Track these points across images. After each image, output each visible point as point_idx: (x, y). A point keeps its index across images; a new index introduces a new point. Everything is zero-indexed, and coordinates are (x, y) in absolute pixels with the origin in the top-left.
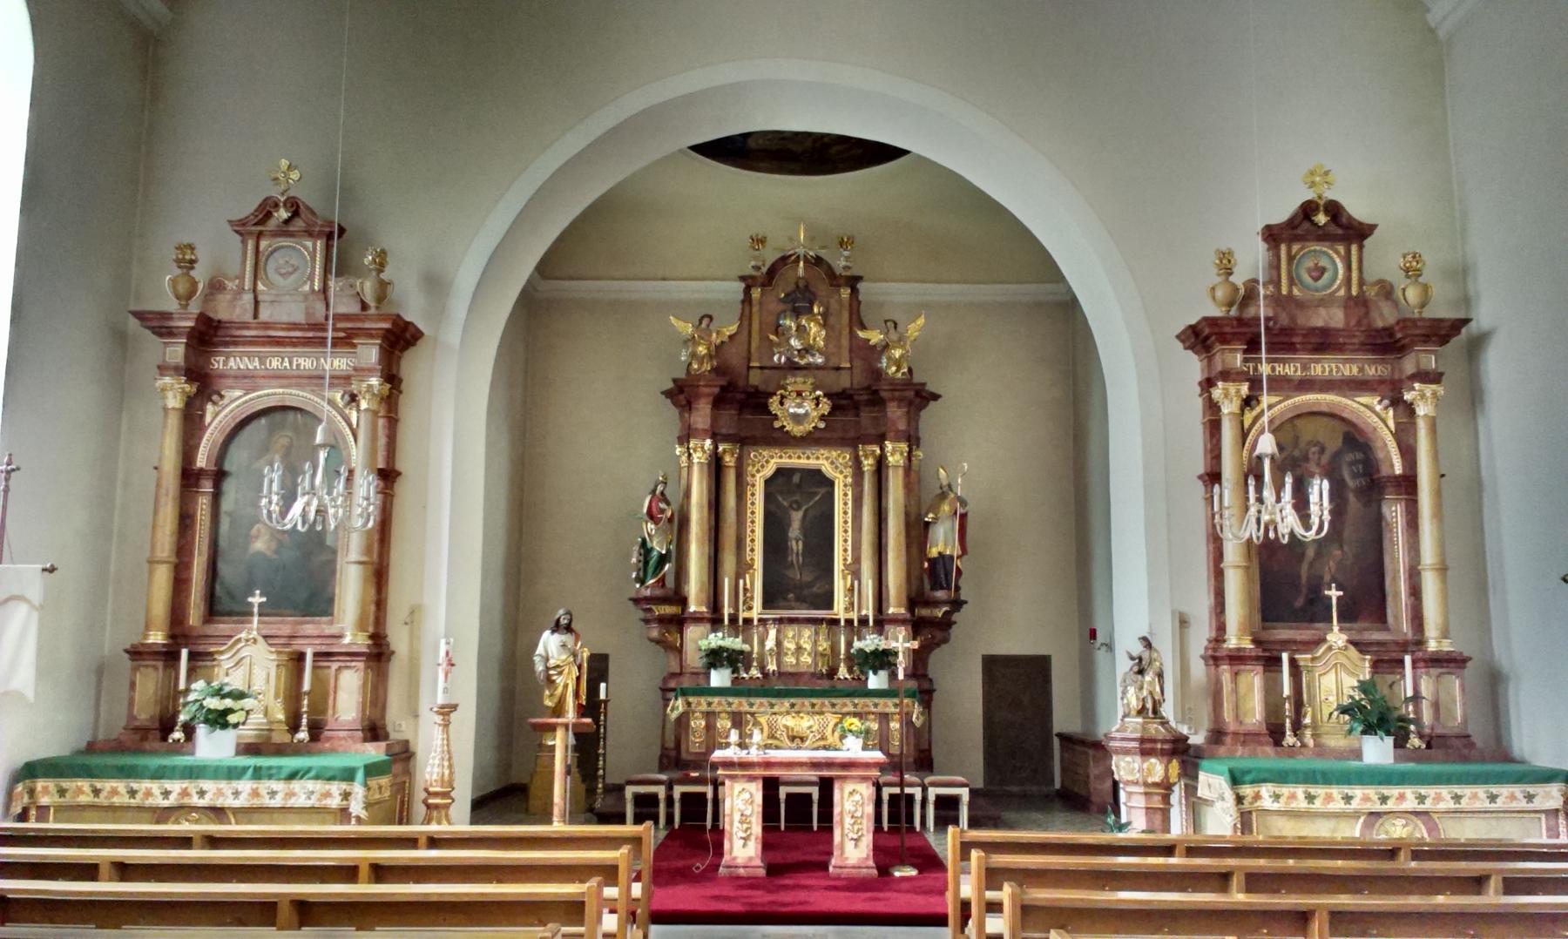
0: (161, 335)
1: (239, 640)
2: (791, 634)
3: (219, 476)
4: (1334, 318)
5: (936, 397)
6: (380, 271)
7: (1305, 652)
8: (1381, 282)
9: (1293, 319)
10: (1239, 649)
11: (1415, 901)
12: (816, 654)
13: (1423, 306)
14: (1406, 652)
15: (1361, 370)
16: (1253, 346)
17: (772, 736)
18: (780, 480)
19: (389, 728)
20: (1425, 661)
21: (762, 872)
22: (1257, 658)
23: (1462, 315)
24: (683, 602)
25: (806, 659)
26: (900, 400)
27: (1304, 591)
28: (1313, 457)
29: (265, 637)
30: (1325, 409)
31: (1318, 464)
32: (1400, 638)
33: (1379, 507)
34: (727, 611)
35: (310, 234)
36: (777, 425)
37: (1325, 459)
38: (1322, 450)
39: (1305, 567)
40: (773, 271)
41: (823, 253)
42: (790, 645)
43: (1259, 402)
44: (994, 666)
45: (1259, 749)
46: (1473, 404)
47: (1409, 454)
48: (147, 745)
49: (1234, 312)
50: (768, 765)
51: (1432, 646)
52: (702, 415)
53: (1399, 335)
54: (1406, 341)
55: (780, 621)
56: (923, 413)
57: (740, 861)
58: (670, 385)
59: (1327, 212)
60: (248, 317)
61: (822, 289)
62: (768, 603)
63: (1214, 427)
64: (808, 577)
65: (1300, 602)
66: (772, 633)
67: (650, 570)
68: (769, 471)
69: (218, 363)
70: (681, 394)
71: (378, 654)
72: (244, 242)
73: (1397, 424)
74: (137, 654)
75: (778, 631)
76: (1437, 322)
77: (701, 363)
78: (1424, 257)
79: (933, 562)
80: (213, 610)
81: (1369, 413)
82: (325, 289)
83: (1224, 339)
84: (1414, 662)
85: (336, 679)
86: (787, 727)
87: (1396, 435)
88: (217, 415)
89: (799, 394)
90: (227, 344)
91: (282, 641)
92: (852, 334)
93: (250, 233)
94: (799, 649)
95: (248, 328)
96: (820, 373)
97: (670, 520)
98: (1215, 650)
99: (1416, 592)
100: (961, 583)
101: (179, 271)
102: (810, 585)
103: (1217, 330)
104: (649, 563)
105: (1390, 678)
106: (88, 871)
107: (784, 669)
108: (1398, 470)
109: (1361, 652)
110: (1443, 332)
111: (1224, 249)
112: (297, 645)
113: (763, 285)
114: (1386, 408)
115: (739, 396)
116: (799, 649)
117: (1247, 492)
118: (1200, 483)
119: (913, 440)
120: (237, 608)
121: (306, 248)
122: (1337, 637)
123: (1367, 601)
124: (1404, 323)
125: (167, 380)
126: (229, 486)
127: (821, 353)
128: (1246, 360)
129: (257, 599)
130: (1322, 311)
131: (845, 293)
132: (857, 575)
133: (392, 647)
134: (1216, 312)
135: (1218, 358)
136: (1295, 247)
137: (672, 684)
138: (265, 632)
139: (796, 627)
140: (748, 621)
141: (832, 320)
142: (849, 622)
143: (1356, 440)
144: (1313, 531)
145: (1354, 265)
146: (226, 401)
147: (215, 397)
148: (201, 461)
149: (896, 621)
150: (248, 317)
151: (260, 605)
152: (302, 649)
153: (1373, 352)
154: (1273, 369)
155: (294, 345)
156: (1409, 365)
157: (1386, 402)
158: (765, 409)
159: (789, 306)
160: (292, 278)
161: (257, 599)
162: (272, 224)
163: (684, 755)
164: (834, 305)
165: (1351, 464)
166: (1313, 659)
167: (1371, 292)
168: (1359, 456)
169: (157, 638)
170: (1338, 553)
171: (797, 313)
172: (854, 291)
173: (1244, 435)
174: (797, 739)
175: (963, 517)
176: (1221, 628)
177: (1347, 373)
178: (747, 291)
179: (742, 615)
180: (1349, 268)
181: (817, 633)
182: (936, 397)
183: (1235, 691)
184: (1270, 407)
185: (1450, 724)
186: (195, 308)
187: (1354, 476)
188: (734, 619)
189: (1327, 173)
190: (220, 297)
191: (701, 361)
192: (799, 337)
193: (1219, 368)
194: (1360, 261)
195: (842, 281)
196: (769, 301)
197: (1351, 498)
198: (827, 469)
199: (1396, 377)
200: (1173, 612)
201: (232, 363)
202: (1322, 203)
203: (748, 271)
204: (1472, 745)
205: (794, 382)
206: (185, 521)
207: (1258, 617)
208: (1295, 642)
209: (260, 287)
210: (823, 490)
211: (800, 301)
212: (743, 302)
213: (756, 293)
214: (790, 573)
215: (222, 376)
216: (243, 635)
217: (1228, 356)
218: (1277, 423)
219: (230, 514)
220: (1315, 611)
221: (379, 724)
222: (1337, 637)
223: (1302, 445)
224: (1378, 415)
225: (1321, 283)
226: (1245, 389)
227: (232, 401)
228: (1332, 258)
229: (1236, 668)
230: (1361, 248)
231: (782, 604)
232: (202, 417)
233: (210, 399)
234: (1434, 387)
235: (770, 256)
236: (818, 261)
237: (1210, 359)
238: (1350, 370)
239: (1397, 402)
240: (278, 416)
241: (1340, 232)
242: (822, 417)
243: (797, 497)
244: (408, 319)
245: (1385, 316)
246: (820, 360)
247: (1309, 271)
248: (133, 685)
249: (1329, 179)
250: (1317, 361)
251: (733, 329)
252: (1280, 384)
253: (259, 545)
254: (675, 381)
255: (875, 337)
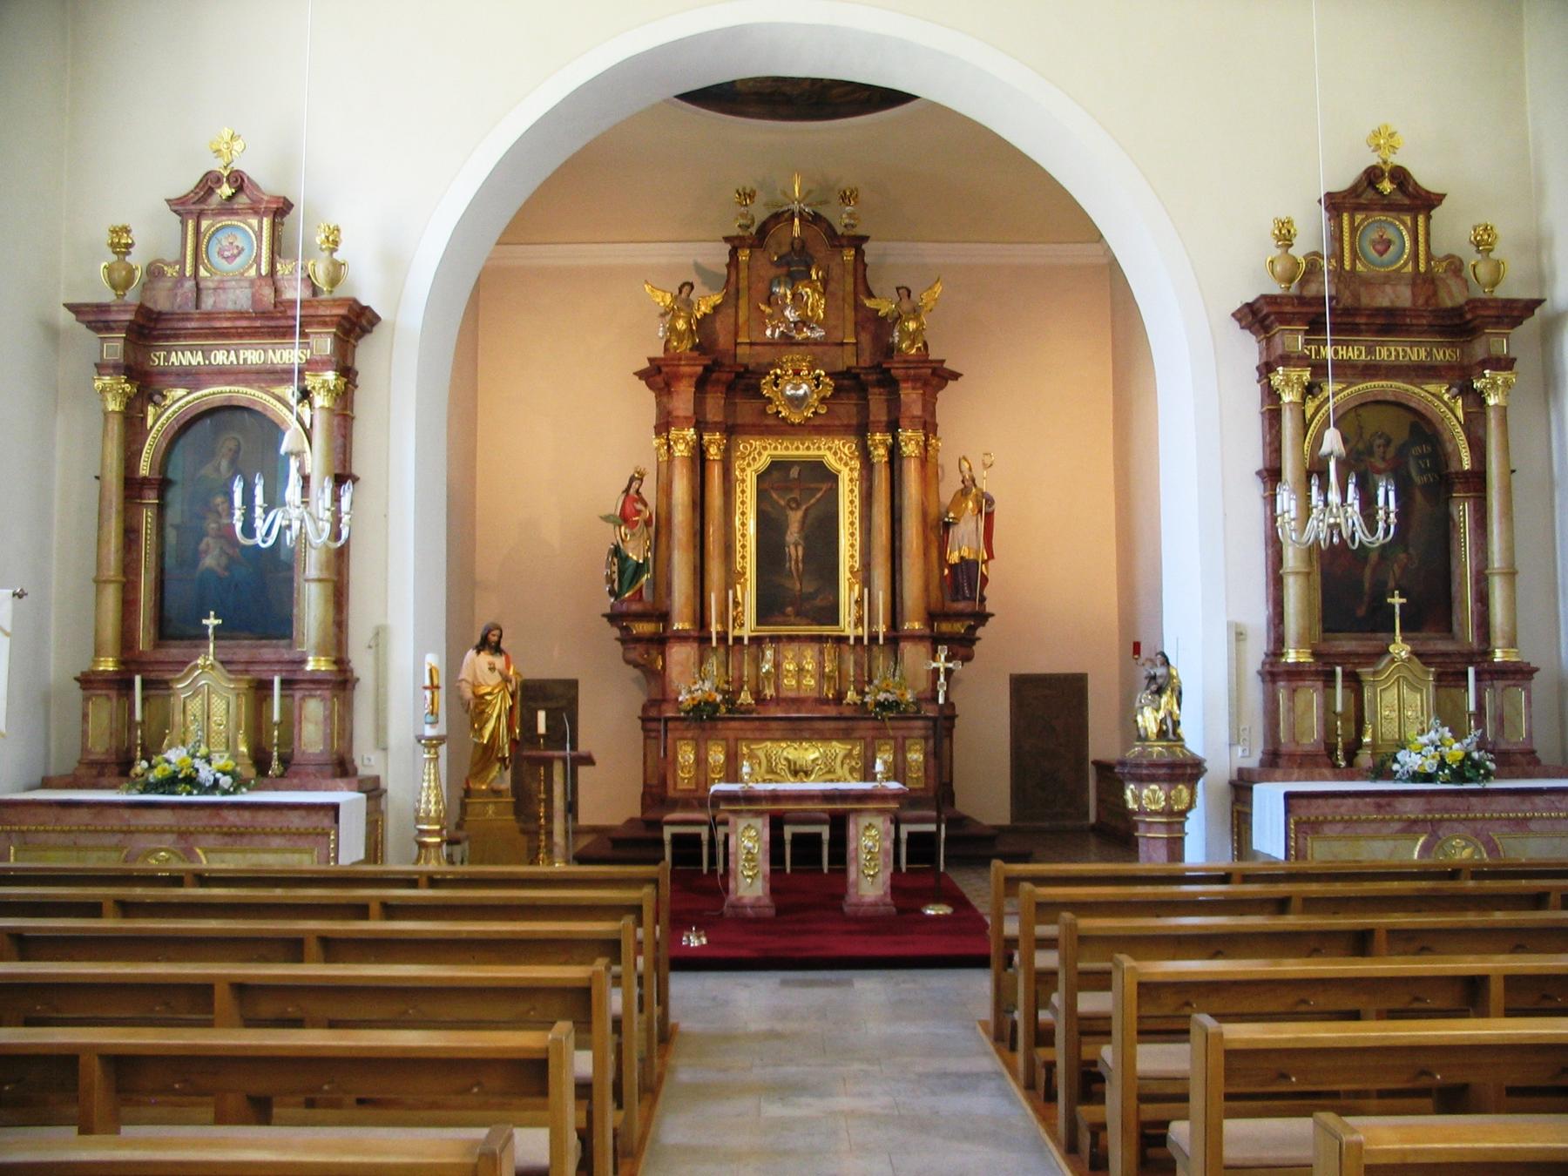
0: (97, 330)
1: (196, 667)
2: (790, 655)
3: (163, 484)
4: (1403, 297)
5: (955, 376)
6: (333, 251)
7: (1368, 664)
8: (1449, 257)
9: (1356, 297)
10: (1298, 664)
11: (1471, 918)
12: (822, 676)
13: (1494, 284)
14: (1471, 664)
15: (1429, 354)
16: (1315, 327)
17: (771, 771)
18: (776, 475)
19: (358, 762)
20: (1489, 672)
21: (771, 912)
22: (1317, 673)
23: (1535, 296)
24: (664, 617)
25: (810, 682)
26: (916, 379)
27: (1366, 599)
28: (1378, 451)
29: (223, 663)
30: (1390, 398)
31: (1383, 459)
32: (1465, 649)
33: (1448, 506)
34: (715, 628)
35: (255, 211)
36: (771, 410)
37: (1391, 451)
38: (1388, 442)
39: (1368, 572)
40: (764, 230)
41: (825, 212)
42: (790, 666)
43: (1321, 390)
44: (1026, 688)
45: (1317, 771)
46: (1546, 394)
47: (1478, 448)
48: (104, 781)
49: (1294, 290)
50: (775, 797)
51: (1499, 656)
52: (683, 402)
53: (1469, 316)
54: (1477, 322)
55: (775, 639)
56: (940, 395)
57: (746, 901)
58: (647, 365)
59: (1393, 179)
60: (190, 308)
61: (821, 250)
62: (762, 618)
63: (1273, 417)
64: (809, 588)
65: (1361, 612)
66: (769, 654)
67: (626, 583)
68: (763, 462)
69: (158, 359)
70: (658, 375)
71: (342, 682)
72: (184, 224)
73: (1466, 414)
74: (88, 681)
75: (776, 652)
76: (1509, 304)
77: (680, 341)
78: (1496, 231)
79: (952, 567)
80: (165, 631)
81: (1437, 403)
82: (273, 271)
83: (1284, 319)
84: (1477, 674)
85: (301, 708)
86: (787, 759)
87: (1466, 428)
88: (159, 417)
89: (797, 373)
90: (167, 338)
91: (241, 667)
92: (858, 306)
93: (190, 213)
94: (801, 670)
95: (188, 319)
96: (818, 349)
97: (648, 523)
98: (1272, 665)
99: (1483, 598)
100: (986, 593)
101: (115, 258)
102: (812, 596)
103: (1276, 309)
104: (625, 572)
105: (1454, 691)
106: (92, 909)
107: (785, 694)
108: (1467, 465)
109: (1424, 664)
110: (1517, 312)
111: (1283, 218)
112: (260, 672)
113: (751, 247)
114: (1454, 397)
115: (724, 377)
116: (801, 670)
117: (1310, 490)
118: (1258, 481)
119: (929, 426)
120: (193, 632)
121: (251, 226)
122: (1400, 649)
123: (1432, 606)
124: (1474, 304)
125: (107, 379)
126: (174, 495)
127: (821, 324)
128: (1307, 342)
129: (212, 622)
130: (1388, 289)
131: (849, 255)
132: (867, 582)
133: (357, 674)
134: (1276, 289)
135: (1277, 339)
136: (1359, 217)
137: (653, 713)
138: (225, 658)
139: (795, 646)
140: (738, 640)
141: (832, 287)
142: (859, 639)
143: (1424, 429)
144: (1381, 533)
145: (1421, 239)
146: (168, 402)
147: (157, 398)
148: (144, 469)
149: (914, 637)
150: (190, 308)
151: (216, 628)
152: (264, 676)
153: (1441, 333)
154: (1336, 352)
155: (240, 336)
156: (1479, 350)
157: (1455, 390)
158: (756, 392)
159: (784, 270)
160: (238, 260)
161: (212, 622)
162: (214, 201)
163: (671, 793)
164: (836, 271)
165: (1422, 457)
166: (1375, 673)
167: (1440, 270)
168: (1426, 449)
169: (108, 665)
170: (1402, 556)
171: (793, 279)
172: (860, 253)
173: (1306, 426)
174: (797, 771)
175: (989, 517)
176: (1278, 642)
177: (1415, 358)
178: (733, 254)
179: (732, 633)
180: (1415, 241)
181: (821, 652)
182: (955, 376)
183: (1291, 710)
184: (1334, 395)
185: (1514, 740)
186: (132, 296)
187: (1422, 472)
188: (723, 638)
189: (1392, 135)
190: (161, 284)
191: (680, 339)
192: (795, 308)
193: (1279, 352)
194: (1428, 234)
195: (844, 242)
196: (764, 264)
197: (1419, 497)
198: (831, 461)
199: (1466, 362)
200: (1229, 625)
201: (173, 359)
202: (1387, 169)
203: (734, 231)
204: (1537, 762)
205: (789, 357)
206: (130, 535)
207: (1318, 628)
208: (1357, 655)
209: (203, 272)
210: (825, 487)
211: (795, 265)
212: (728, 266)
213: (744, 256)
214: (788, 584)
215: (164, 373)
216: (200, 661)
217: (1288, 338)
218: (1341, 412)
219: (177, 527)
220: (1379, 621)
221: (347, 756)
222: (1400, 649)
223: (1367, 436)
224: (1446, 404)
225: (1386, 257)
226: (1306, 375)
227: (175, 402)
228: (1399, 229)
229: (1294, 685)
230: (1428, 218)
231: (780, 619)
232: (144, 419)
233: (150, 400)
234: (1505, 374)
235: (760, 214)
236: (817, 218)
237: (1269, 340)
238: (1418, 354)
239: (1466, 390)
240: (226, 415)
241: (1407, 201)
242: (823, 400)
243: (795, 494)
244: (364, 303)
245: (1452, 296)
246: (819, 333)
247: (1374, 243)
248: (85, 716)
249: (1393, 142)
250: (1382, 344)
251: (717, 299)
252: (1345, 370)
253: (209, 561)
254: (651, 360)
255: (885, 307)
